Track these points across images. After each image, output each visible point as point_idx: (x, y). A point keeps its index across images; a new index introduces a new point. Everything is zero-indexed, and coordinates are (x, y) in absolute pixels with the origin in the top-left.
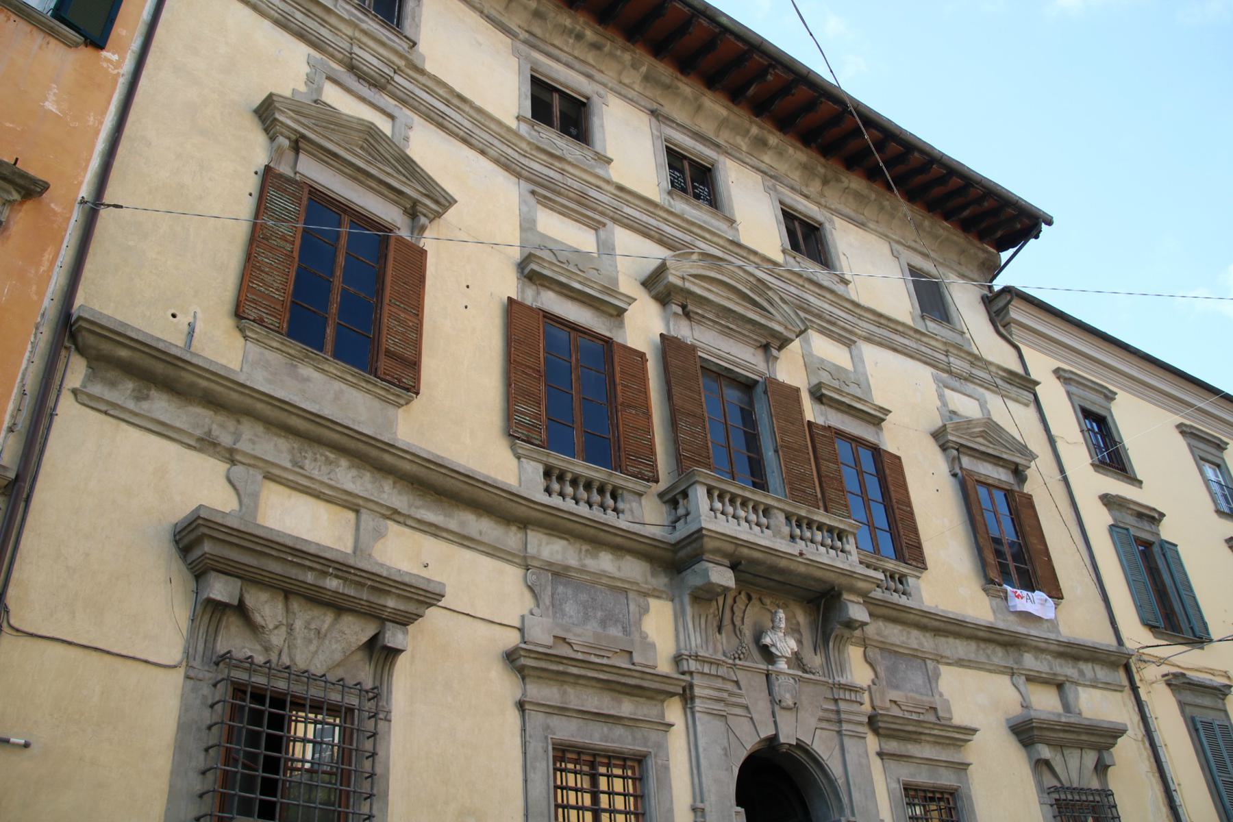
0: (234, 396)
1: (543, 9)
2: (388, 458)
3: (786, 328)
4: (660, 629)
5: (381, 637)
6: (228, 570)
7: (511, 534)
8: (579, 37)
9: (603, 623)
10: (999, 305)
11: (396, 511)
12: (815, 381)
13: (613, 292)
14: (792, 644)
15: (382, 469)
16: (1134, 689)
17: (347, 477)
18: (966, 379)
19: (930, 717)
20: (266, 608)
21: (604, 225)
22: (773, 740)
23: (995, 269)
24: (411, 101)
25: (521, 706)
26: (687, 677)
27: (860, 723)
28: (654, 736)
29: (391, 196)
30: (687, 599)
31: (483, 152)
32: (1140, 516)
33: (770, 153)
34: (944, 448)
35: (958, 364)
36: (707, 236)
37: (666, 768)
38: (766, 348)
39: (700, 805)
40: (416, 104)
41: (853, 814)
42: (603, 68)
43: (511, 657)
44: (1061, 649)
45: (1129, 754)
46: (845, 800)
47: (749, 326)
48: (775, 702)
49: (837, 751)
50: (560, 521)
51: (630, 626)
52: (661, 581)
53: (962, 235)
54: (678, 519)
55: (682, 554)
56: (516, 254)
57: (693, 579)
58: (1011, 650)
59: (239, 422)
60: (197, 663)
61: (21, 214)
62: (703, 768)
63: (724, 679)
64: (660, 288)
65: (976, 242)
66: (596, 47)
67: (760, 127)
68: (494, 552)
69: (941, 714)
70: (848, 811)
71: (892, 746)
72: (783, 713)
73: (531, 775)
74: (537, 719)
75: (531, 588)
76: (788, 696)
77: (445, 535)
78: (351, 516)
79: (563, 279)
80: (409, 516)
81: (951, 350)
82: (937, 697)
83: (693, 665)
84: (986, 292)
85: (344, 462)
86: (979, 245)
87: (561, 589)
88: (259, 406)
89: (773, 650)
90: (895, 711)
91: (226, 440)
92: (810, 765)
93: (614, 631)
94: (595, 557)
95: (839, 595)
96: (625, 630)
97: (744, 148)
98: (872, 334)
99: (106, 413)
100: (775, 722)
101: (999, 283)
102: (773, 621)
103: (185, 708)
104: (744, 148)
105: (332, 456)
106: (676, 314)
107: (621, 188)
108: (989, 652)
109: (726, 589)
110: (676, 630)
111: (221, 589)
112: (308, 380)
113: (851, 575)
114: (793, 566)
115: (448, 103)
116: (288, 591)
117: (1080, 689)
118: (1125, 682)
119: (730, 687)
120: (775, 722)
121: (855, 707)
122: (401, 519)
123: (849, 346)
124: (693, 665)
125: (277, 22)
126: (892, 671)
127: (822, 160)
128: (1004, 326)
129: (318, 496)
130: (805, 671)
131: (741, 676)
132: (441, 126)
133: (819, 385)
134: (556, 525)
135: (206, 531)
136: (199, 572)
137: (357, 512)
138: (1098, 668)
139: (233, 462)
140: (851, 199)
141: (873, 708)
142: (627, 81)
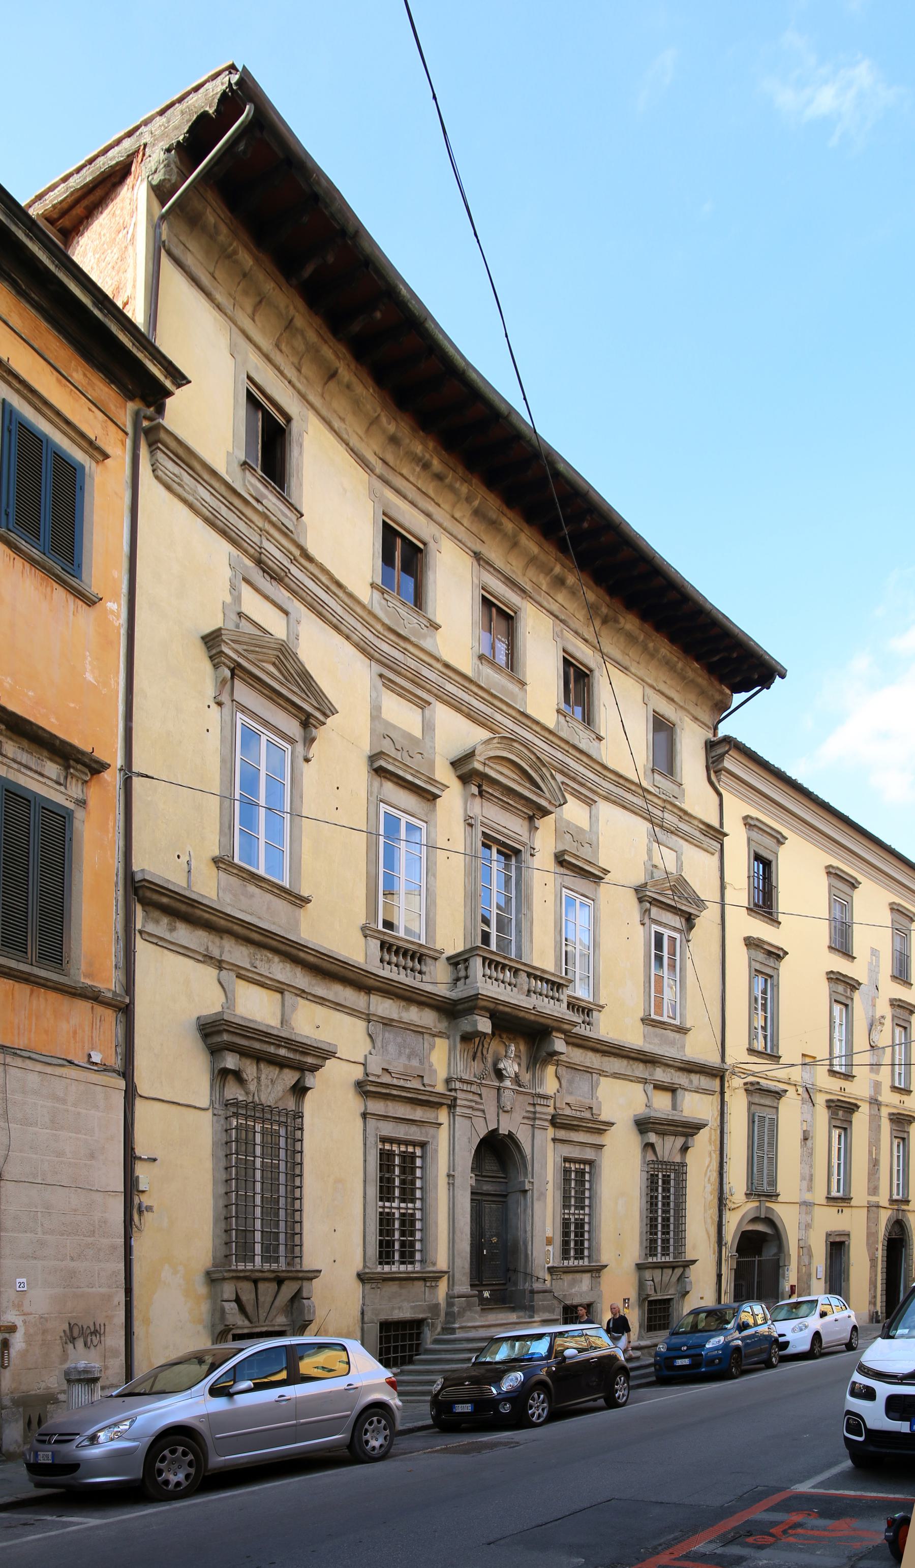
0: (222, 922)
1: (399, 435)
2: (302, 955)
3: (550, 802)
4: (440, 1061)
5: (302, 1080)
6: (232, 1048)
7: (361, 997)
8: (426, 466)
9: (409, 1057)
10: (718, 750)
11: (304, 991)
12: (561, 848)
13: (432, 781)
14: (516, 1068)
15: (295, 961)
16: (722, 1093)
17: (281, 971)
18: (672, 832)
19: (587, 1115)
20: (250, 1070)
21: (430, 704)
22: (496, 1130)
23: (721, 708)
24: (301, 592)
25: (364, 1115)
26: (453, 1094)
27: (546, 1120)
28: (431, 1131)
29: (293, 710)
30: (458, 1039)
31: (348, 638)
32: (770, 953)
33: (564, 591)
34: (641, 900)
35: (670, 819)
36: (504, 708)
37: (436, 1151)
38: (531, 819)
39: (452, 1173)
40: (304, 594)
41: (533, 1178)
42: (440, 502)
43: (359, 1085)
44: (682, 1065)
45: (703, 1142)
46: (530, 1169)
47: (523, 802)
48: (501, 1108)
49: (530, 1139)
50: (214, 918)
51: (424, 1059)
52: (442, 1026)
53: (706, 677)
54: (458, 979)
55: (460, 1007)
56: (366, 749)
57: (465, 1025)
58: (649, 1065)
59: (221, 938)
60: (217, 1106)
61: (92, 790)
62: (456, 1151)
63: (474, 1093)
64: (465, 769)
65: (716, 683)
66: (439, 477)
67: (563, 565)
68: (352, 1012)
69: (594, 1112)
70: (530, 1176)
71: (562, 1134)
72: (504, 1114)
73: (368, 1158)
74: (371, 1123)
75: (370, 1036)
76: (509, 1103)
77: (327, 1003)
78: (278, 996)
79: (401, 773)
80: (310, 994)
81: (668, 806)
82: (594, 1099)
83: (458, 1085)
84: (710, 735)
85: (276, 959)
86: (718, 687)
87: (387, 1035)
88: (236, 927)
89: (504, 1072)
90: (568, 1112)
91: (216, 953)
92: (513, 1147)
93: (415, 1063)
94: (407, 1010)
95: (551, 1033)
96: (422, 1063)
97: (544, 587)
98: (610, 792)
99: (156, 944)
100: (498, 1120)
101: (725, 729)
102: (506, 1052)
103: (215, 1133)
104: (544, 587)
105: (270, 956)
106: (473, 795)
107: (447, 666)
108: (634, 1067)
109: (487, 1034)
110: (449, 1059)
111: (231, 1061)
112: (252, 896)
113: (561, 1020)
114: (527, 1016)
115: (327, 589)
116: (259, 1058)
117: (686, 1093)
118: (718, 1089)
119: (477, 1098)
120: (498, 1120)
121: (544, 1110)
122: (305, 996)
123: (590, 805)
124: (458, 1085)
125: (207, 520)
126: (571, 1082)
127: (607, 598)
128: (715, 772)
129: (262, 985)
130: (520, 1086)
131: (484, 1091)
132: (320, 615)
133: (564, 852)
134: (390, 990)
135: (226, 1027)
136: (215, 1051)
137: (282, 993)
138: (702, 1078)
139: (221, 968)
140: (622, 640)
141: (555, 1108)
142: (458, 515)
